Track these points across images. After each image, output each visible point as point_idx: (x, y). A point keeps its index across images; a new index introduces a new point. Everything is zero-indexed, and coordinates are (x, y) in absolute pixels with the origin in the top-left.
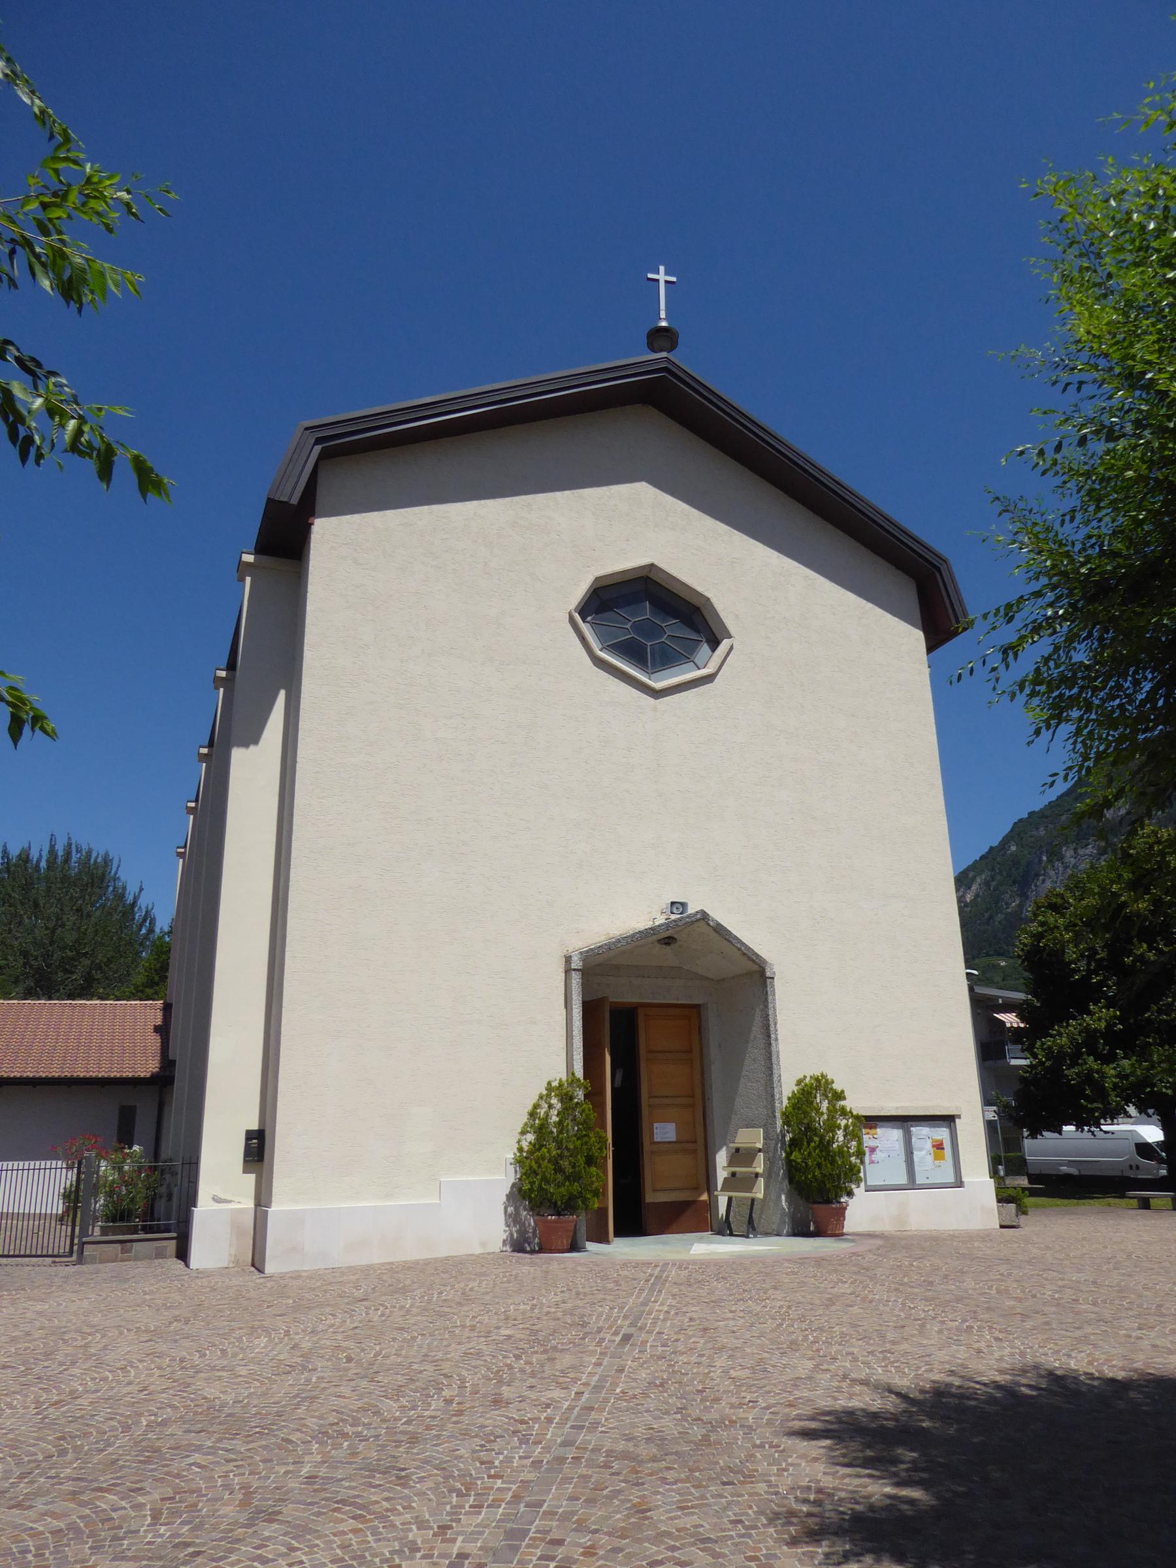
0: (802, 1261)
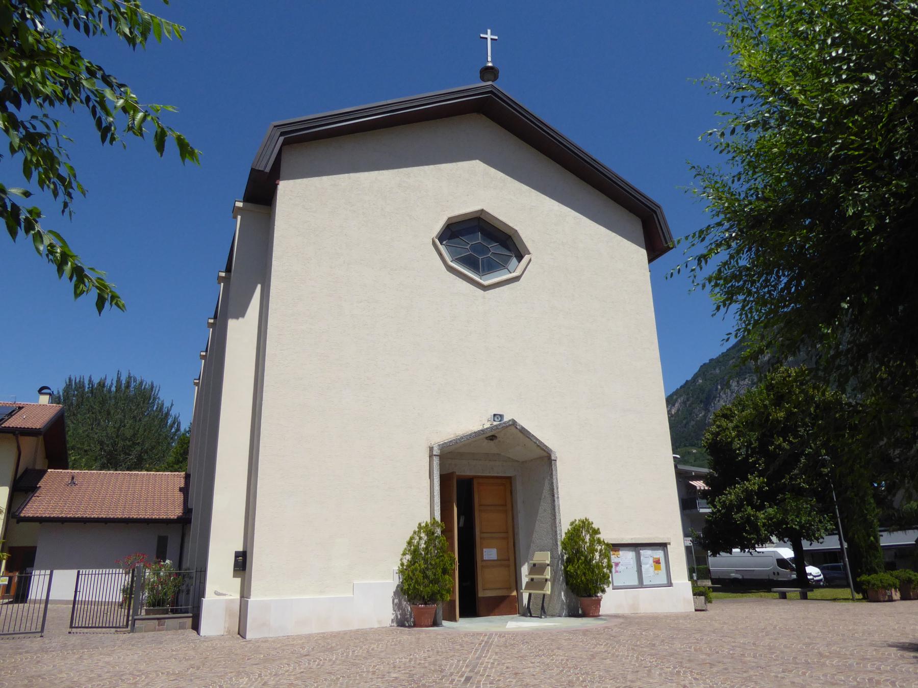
0: (574, 632)
